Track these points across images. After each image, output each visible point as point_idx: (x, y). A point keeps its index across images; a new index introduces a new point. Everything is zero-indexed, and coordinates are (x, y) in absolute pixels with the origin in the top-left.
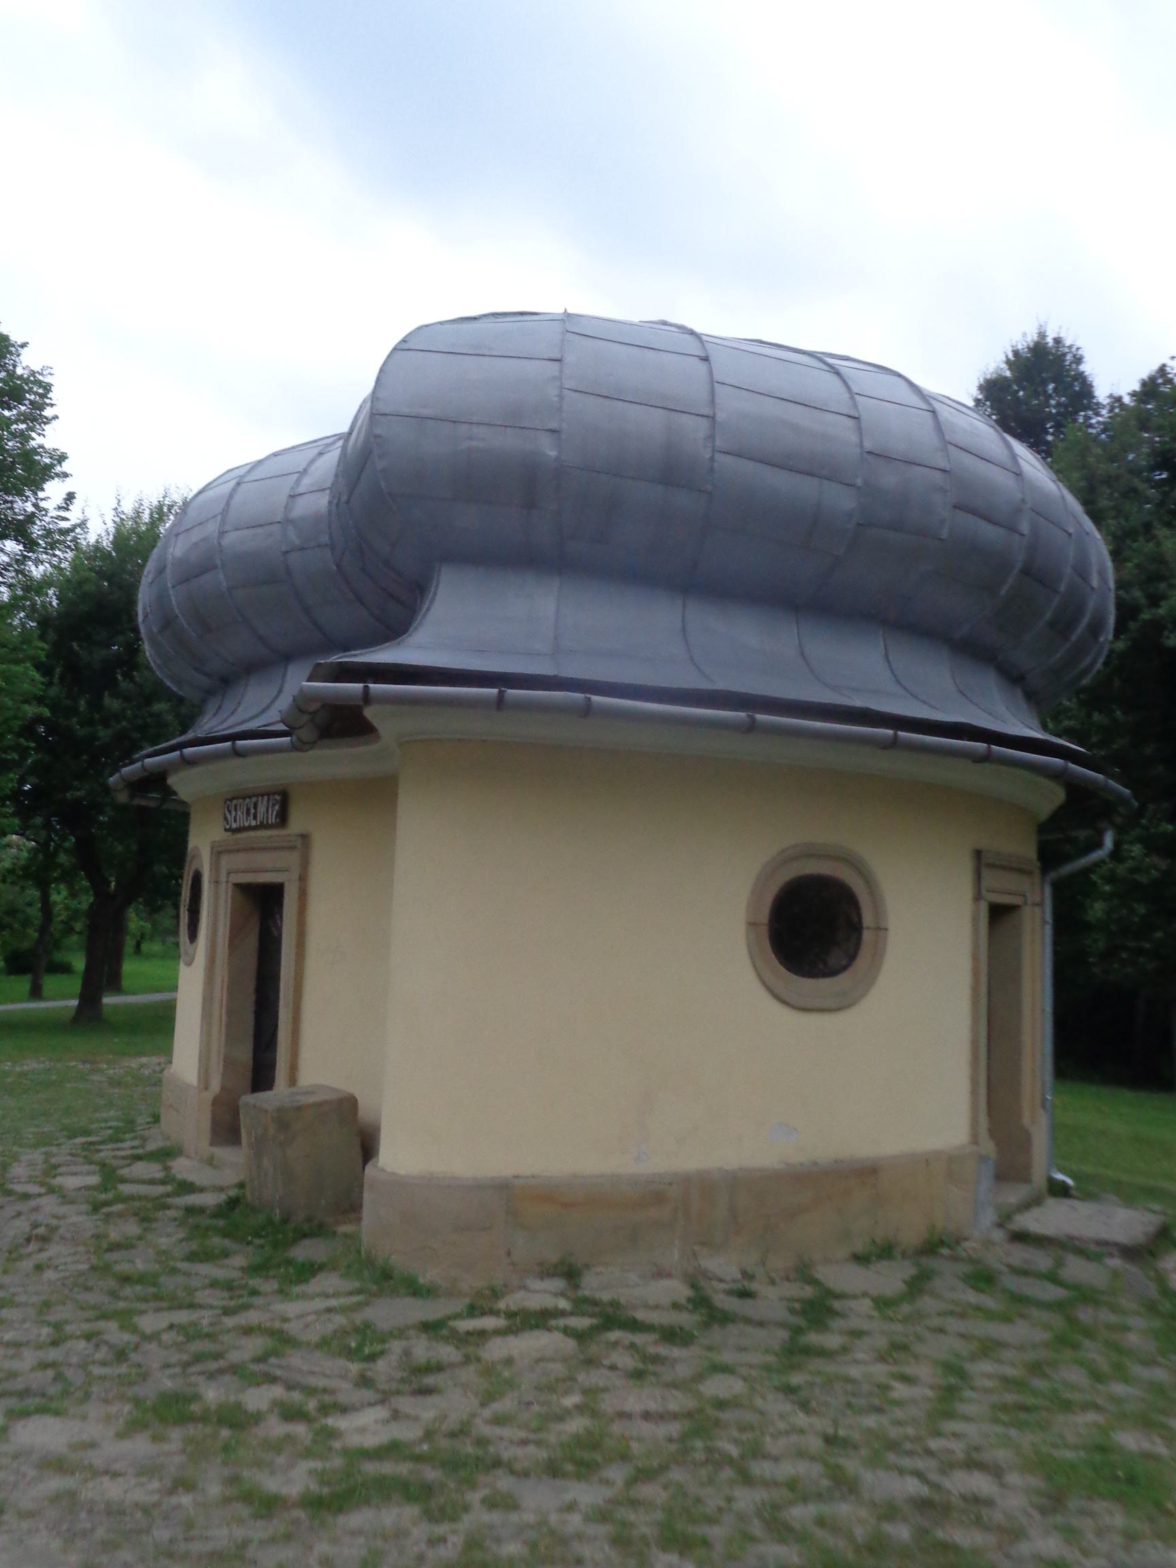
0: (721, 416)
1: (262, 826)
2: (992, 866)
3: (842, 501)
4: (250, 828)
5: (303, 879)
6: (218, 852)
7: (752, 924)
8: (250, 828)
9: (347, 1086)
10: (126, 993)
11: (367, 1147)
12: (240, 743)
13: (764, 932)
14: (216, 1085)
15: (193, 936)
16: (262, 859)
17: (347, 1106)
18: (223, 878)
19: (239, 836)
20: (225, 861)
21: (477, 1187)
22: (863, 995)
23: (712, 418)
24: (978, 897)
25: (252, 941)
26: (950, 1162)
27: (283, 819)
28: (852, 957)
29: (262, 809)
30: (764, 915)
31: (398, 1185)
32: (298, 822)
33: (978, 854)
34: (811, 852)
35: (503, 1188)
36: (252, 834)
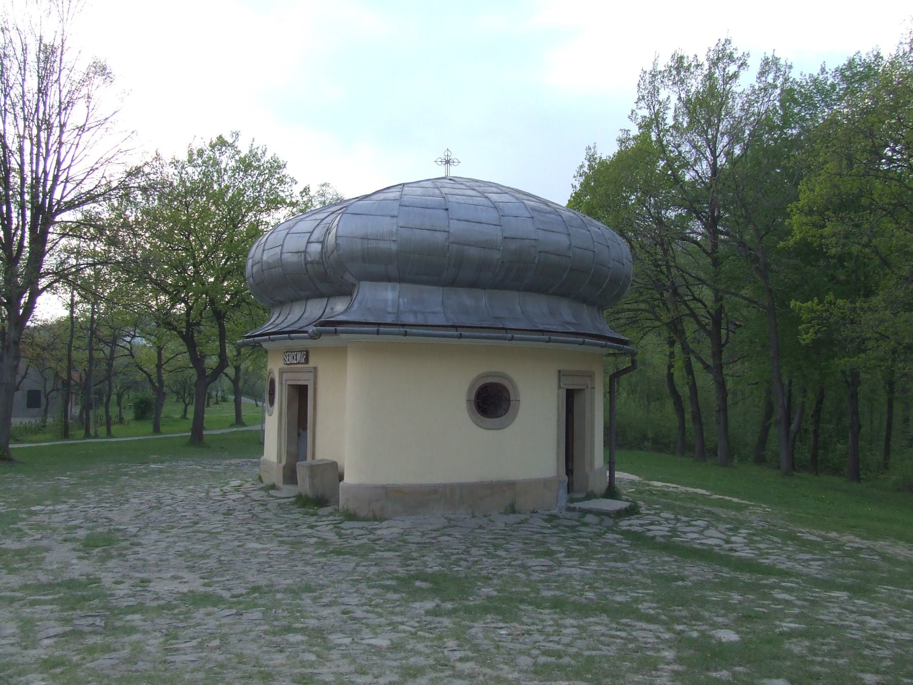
0: (451, 231)
1: (299, 363)
2: (563, 375)
3: (497, 255)
4: (294, 364)
5: (315, 384)
6: (281, 372)
7: (468, 400)
8: (294, 364)
9: (335, 459)
10: (246, 426)
11: (341, 478)
12: (291, 335)
13: (473, 403)
14: (284, 462)
15: (272, 403)
16: (300, 376)
17: (334, 465)
18: (284, 382)
19: (290, 366)
20: (285, 376)
21: (376, 487)
22: (508, 426)
23: (448, 232)
24: (559, 387)
25: (296, 406)
26: (545, 483)
27: (307, 361)
28: (506, 411)
29: (298, 357)
30: (473, 397)
31: (350, 487)
32: (312, 363)
33: (560, 371)
34: (488, 375)
35: (384, 487)
36: (295, 366)
